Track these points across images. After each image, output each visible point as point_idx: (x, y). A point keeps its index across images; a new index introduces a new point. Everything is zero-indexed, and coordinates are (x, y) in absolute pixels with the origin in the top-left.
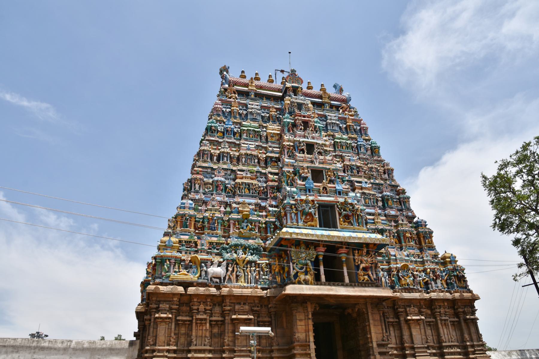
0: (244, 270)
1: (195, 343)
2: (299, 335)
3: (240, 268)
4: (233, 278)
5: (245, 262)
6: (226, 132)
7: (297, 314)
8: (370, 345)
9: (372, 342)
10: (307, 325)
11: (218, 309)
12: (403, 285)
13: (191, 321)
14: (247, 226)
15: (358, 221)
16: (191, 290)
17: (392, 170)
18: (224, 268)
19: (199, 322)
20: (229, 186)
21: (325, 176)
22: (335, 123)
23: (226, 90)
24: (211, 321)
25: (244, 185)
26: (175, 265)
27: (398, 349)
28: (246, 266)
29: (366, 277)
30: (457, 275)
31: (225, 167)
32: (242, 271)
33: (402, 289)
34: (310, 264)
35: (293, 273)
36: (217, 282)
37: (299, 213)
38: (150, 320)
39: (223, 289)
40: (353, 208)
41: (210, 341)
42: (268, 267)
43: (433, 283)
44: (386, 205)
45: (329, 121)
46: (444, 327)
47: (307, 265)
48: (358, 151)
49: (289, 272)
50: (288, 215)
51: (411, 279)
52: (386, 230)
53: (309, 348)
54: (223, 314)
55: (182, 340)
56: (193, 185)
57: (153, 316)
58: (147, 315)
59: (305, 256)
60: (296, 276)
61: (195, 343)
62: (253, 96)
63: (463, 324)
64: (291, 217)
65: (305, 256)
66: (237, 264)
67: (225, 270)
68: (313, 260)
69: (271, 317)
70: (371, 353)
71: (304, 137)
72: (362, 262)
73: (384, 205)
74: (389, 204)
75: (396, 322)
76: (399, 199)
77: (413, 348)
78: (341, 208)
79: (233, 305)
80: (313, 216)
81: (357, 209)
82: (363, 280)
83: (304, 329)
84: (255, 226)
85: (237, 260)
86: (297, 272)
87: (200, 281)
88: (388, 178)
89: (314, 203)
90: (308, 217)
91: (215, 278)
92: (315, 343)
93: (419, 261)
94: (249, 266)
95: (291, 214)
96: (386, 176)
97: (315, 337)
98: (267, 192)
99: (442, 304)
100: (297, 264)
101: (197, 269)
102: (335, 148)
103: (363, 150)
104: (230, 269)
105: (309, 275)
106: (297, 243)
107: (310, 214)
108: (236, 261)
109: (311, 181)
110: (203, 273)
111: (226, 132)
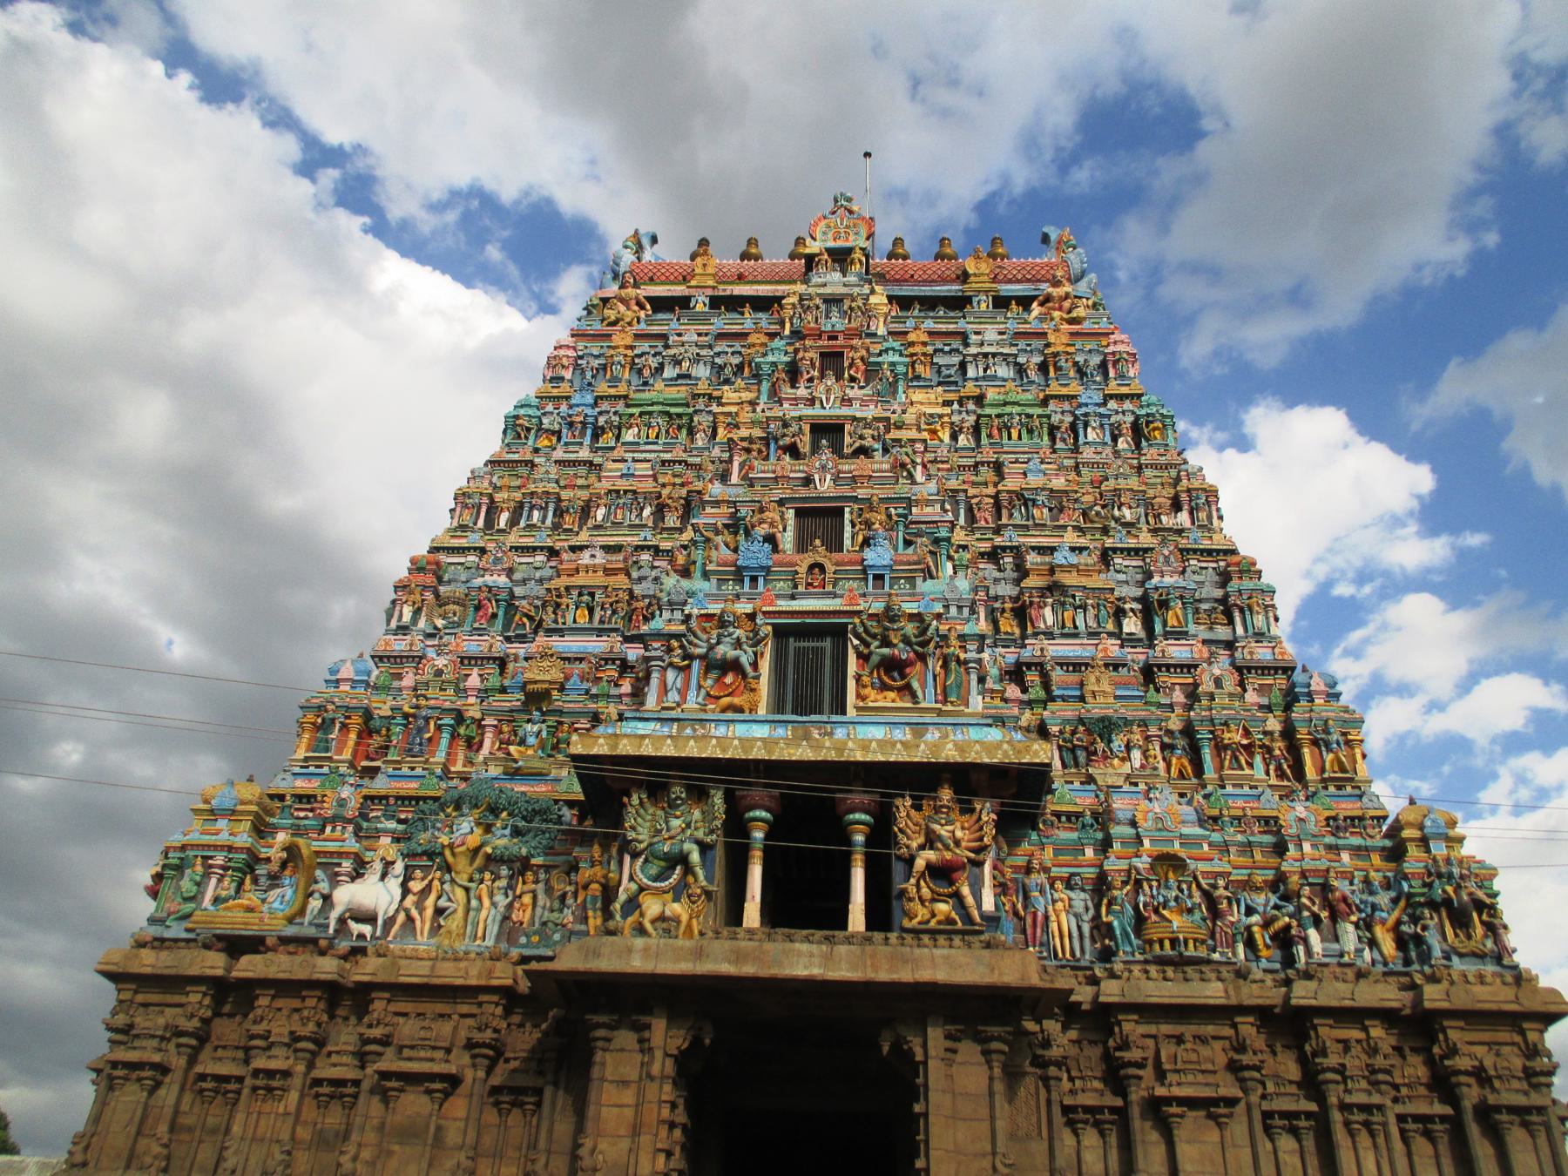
0: (467, 890)
3: (453, 881)
4: (424, 924)
5: (479, 861)
12: (1150, 942)
18: (394, 885)
20: (524, 603)
22: (994, 355)
28: (477, 876)
30: (1447, 902)
32: (460, 893)
33: (1146, 962)
36: (361, 936)
43: (1313, 934)
46: (1364, 1139)
47: (683, 859)
50: (655, 675)
51: (1197, 916)
52: (1128, 723)
59: (687, 826)
63: (1474, 1130)
64: (664, 683)
66: (448, 868)
67: (398, 892)
71: (811, 401)
74: (1172, 621)
75: (1113, 1110)
76: (1223, 601)
80: (745, 676)
85: (447, 853)
87: (291, 931)
88: (1187, 524)
90: (729, 679)
91: (358, 920)
93: (1260, 844)
99: (1356, 1034)
102: (978, 439)
104: (416, 886)
105: (685, 899)
107: (734, 666)
108: (442, 854)
110: (315, 903)
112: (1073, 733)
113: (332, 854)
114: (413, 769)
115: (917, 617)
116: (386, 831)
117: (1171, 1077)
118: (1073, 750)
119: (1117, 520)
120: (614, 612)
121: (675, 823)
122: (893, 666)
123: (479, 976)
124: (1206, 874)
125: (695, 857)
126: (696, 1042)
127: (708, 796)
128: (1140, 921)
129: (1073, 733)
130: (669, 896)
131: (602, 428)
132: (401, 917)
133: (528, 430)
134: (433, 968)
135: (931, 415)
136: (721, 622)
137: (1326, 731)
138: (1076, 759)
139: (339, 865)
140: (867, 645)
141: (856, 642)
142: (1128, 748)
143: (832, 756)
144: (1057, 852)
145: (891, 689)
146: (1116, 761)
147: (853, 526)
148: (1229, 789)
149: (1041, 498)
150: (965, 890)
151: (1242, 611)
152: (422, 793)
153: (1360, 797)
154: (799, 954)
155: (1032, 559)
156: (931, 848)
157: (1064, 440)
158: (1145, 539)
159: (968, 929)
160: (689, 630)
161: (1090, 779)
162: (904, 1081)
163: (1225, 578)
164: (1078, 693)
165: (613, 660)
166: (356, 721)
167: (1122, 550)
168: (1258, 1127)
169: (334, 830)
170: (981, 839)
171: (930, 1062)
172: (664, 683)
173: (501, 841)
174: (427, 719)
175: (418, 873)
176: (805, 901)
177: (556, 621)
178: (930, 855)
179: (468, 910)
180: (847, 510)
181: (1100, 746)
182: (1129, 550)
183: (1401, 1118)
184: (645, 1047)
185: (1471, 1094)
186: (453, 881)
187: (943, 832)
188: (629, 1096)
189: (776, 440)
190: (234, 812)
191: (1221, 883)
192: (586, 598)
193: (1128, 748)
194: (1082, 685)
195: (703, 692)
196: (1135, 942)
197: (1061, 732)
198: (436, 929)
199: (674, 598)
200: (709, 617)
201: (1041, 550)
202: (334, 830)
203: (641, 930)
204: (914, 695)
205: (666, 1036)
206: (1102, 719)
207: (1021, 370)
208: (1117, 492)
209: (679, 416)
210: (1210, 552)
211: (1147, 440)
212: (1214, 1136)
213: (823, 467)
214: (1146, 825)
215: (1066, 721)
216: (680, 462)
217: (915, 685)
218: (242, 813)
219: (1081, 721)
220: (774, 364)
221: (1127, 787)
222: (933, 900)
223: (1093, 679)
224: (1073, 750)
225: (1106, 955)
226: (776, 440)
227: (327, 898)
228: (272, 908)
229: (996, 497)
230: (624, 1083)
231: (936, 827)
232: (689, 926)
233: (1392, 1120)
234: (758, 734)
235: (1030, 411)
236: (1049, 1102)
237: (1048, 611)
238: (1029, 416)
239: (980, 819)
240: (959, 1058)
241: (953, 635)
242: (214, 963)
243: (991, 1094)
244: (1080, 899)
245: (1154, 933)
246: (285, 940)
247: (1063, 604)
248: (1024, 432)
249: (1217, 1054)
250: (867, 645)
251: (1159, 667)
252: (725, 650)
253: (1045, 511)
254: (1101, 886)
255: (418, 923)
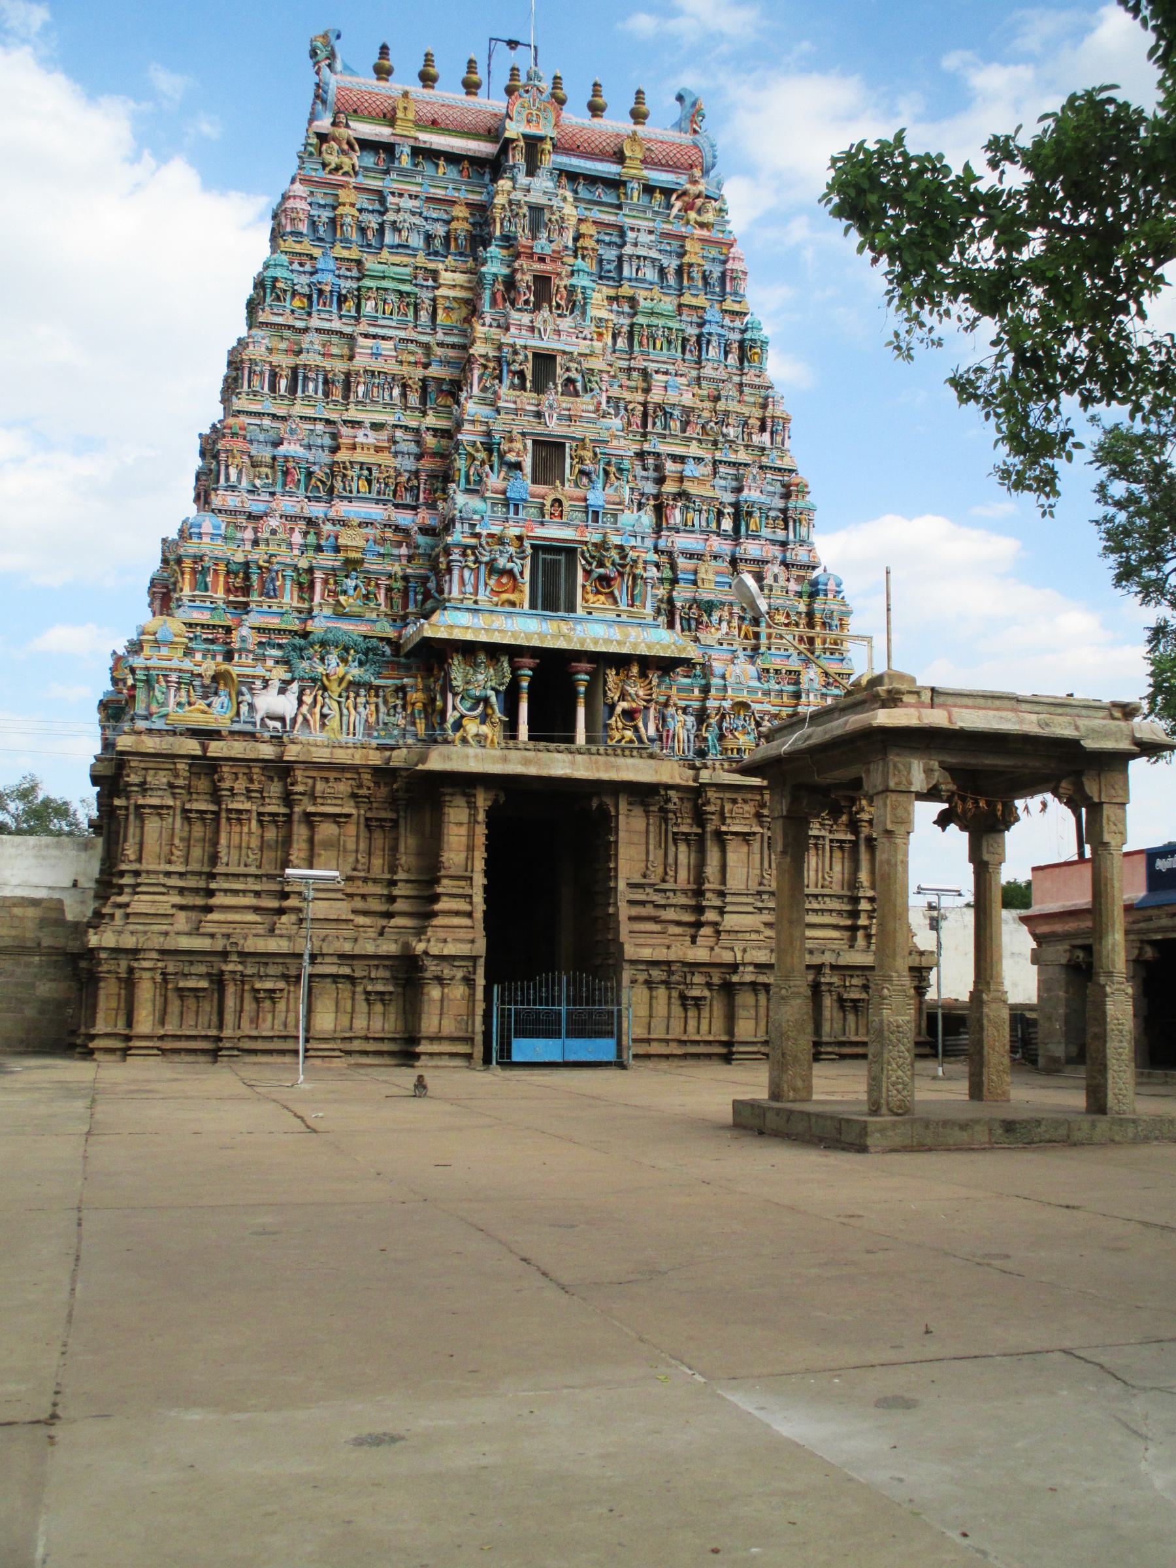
0: (339, 703)
1: (225, 860)
2: (452, 855)
3: (330, 697)
4: (315, 720)
5: (344, 685)
6: (315, 296)
7: (451, 811)
8: (612, 884)
9: (616, 877)
10: (471, 835)
11: (276, 789)
12: (727, 749)
13: (217, 814)
14: (356, 588)
15: (633, 591)
16: (216, 748)
17: (786, 420)
19: (233, 816)
21: (568, 461)
22: (645, 258)
23: (323, 138)
24: (260, 814)
25: (357, 467)
26: (178, 689)
27: (690, 894)
28: (344, 694)
29: (629, 734)
31: (309, 412)
32: (335, 705)
34: (493, 699)
35: (451, 716)
37: (483, 567)
38: (127, 808)
39: (291, 747)
40: (624, 557)
41: (258, 856)
42: (400, 695)
44: (743, 529)
45: (628, 250)
47: (486, 700)
48: (700, 356)
49: (443, 712)
50: (456, 573)
51: (752, 737)
52: (723, 604)
53: (471, 885)
54: (288, 799)
55: (197, 852)
56: (223, 468)
57: (132, 801)
58: (119, 797)
59: (485, 680)
60: (458, 725)
61: (225, 860)
62: (405, 161)
63: (863, 849)
64: (462, 577)
65: (485, 680)
66: (325, 688)
67: (296, 703)
68: (502, 688)
69: (397, 812)
70: (612, 901)
72: (623, 696)
73: (737, 529)
74: (752, 527)
75: (696, 834)
76: (784, 511)
77: (722, 894)
78: (593, 557)
79: (310, 781)
80: (515, 579)
81: (635, 562)
82: (619, 741)
83: (463, 839)
84: (377, 585)
85: (324, 679)
86: (462, 717)
87: (237, 727)
88: (768, 445)
89: (522, 545)
90: (504, 580)
92: (487, 874)
94: (352, 695)
95: (462, 568)
96: (766, 437)
97: (487, 862)
98: (418, 488)
100: (462, 698)
101: (230, 699)
103: (713, 352)
104: (308, 699)
106: (469, 649)
107: (510, 573)
109: (529, 481)
110: (244, 709)
111: (315, 296)
112: (690, 608)
113: (248, 676)
114: (270, 607)
115: (621, 548)
116: (271, 656)
117: (728, 821)
118: (688, 620)
119: (724, 435)
120: (387, 485)
121: (481, 677)
122: (605, 580)
123: (361, 759)
124: (760, 712)
125: (493, 699)
126: (495, 801)
127: (498, 660)
128: (721, 737)
129: (690, 608)
130: (478, 721)
131: (345, 296)
132: (300, 719)
133: (285, 291)
134: (332, 753)
135: (600, 319)
136: (500, 540)
137: (831, 618)
138: (689, 625)
139: (254, 683)
140: (590, 564)
141: (583, 562)
142: (720, 621)
143: (578, 647)
144: (679, 690)
145: (601, 593)
146: (713, 630)
147: (572, 458)
148: (773, 651)
149: (676, 413)
150: (641, 724)
151: (795, 521)
152: (283, 627)
153: (842, 660)
154: (558, 761)
155: (670, 466)
156: (624, 700)
157: (691, 351)
158: (743, 456)
159: (640, 748)
160: (481, 545)
161: (696, 640)
162: (605, 824)
163: (787, 496)
164: (692, 577)
165: (390, 526)
166: (222, 568)
167: (725, 462)
168: (766, 845)
169: (240, 657)
170: (650, 695)
171: (620, 817)
172: (462, 577)
173: (355, 672)
174: (277, 572)
175: (308, 691)
176: (552, 725)
177: (344, 489)
178: (624, 705)
179: (341, 715)
180: (567, 445)
181: (705, 618)
182: (730, 463)
183: (831, 841)
184: (472, 806)
185: (865, 831)
186: (330, 697)
187: (632, 691)
188: (463, 830)
189: (509, 364)
190: (172, 643)
191: (767, 718)
192: (366, 472)
193: (720, 621)
194: (695, 572)
195: (489, 589)
196: (719, 748)
197: (683, 607)
198: (323, 725)
199: (464, 515)
200: (491, 536)
201: (675, 458)
202: (240, 657)
203: (464, 740)
204: (615, 602)
205: (482, 801)
206: (708, 602)
207: (662, 272)
208: (727, 413)
209: (408, 294)
210: (780, 470)
211: (749, 362)
212: (745, 849)
213: (551, 406)
214: (731, 680)
215: (686, 600)
216: (412, 341)
217: (617, 593)
218: (177, 643)
219: (695, 600)
220: (495, 275)
221: (717, 646)
222: (624, 729)
223: (703, 570)
224: (688, 620)
225: (702, 753)
226: (509, 364)
227: (251, 706)
228: (218, 712)
229: (645, 405)
230: (461, 824)
231: (628, 688)
232: (492, 741)
233: (827, 842)
234: (529, 628)
235: (671, 324)
236: (666, 831)
237: (677, 512)
238: (670, 329)
239: (650, 683)
240: (632, 814)
241: (641, 561)
242: (192, 746)
243: (647, 832)
244: (691, 720)
245: (729, 743)
246: (232, 733)
247: (688, 508)
248: (665, 345)
249: (749, 809)
250: (590, 564)
251: (741, 560)
252: (502, 562)
253: (678, 423)
254: (702, 717)
255: (312, 723)
